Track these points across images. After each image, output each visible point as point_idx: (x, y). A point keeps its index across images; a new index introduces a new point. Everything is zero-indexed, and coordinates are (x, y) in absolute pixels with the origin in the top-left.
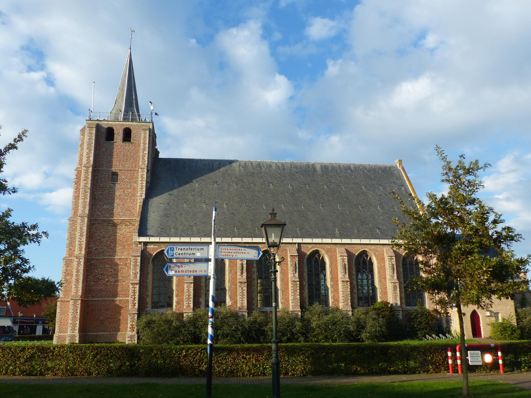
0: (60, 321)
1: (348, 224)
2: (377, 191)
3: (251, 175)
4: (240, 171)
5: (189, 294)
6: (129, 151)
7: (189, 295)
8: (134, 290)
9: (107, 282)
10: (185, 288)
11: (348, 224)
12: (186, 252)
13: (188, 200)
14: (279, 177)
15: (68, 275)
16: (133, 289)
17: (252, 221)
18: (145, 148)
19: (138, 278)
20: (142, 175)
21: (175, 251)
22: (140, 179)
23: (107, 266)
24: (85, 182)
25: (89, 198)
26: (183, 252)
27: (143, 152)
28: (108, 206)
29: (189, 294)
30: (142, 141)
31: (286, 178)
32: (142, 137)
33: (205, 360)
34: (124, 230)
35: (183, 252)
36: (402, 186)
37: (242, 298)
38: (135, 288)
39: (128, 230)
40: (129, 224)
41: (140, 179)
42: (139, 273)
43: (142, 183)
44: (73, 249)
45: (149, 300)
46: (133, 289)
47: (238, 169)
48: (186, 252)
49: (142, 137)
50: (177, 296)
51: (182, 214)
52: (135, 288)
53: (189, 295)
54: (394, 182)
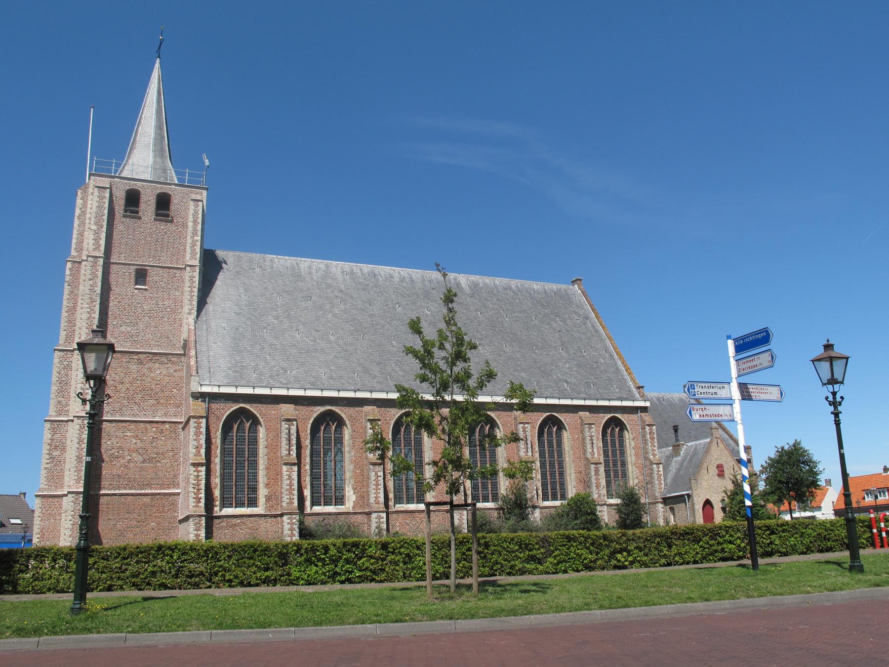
0: (42, 531)
1: (523, 374)
2: (554, 325)
3: (364, 290)
4: (345, 280)
5: (291, 482)
6: (166, 233)
7: (291, 485)
8: (198, 476)
9: (129, 461)
10: (285, 473)
11: (523, 374)
12: (708, 390)
13: (269, 325)
14: (408, 295)
15: (56, 447)
16: (196, 473)
17: (379, 364)
18: (195, 230)
19: (204, 455)
20: (192, 278)
21: (696, 390)
22: (187, 284)
23: (129, 434)
24: (91, 282)
25: (98, 313)
26: (704, 390)
27: (192, 237)
28: (129, 329)
29: (291, 482)
30: (191, 219)
31: (418, 297)
32: (191, 211)
33: (142, 576)
34: (158, 372)
35: (704, 390)
36: (587, 318)
37: (377, 489)
38: (201, 471)
39: (164, 372)
40: (166, 361)
41: (187, 284)
42: (204, 446)
43: (192, 292)
44: (64, 403)
45: (217, 493)
46: (196, 473)
47: (341, 278)
48: (708, 390)
49: (191, 211)
50: (267, 485)
51: (264, 348)
52: (199, 472)
53: (291, 485)
54: (575, 312)
